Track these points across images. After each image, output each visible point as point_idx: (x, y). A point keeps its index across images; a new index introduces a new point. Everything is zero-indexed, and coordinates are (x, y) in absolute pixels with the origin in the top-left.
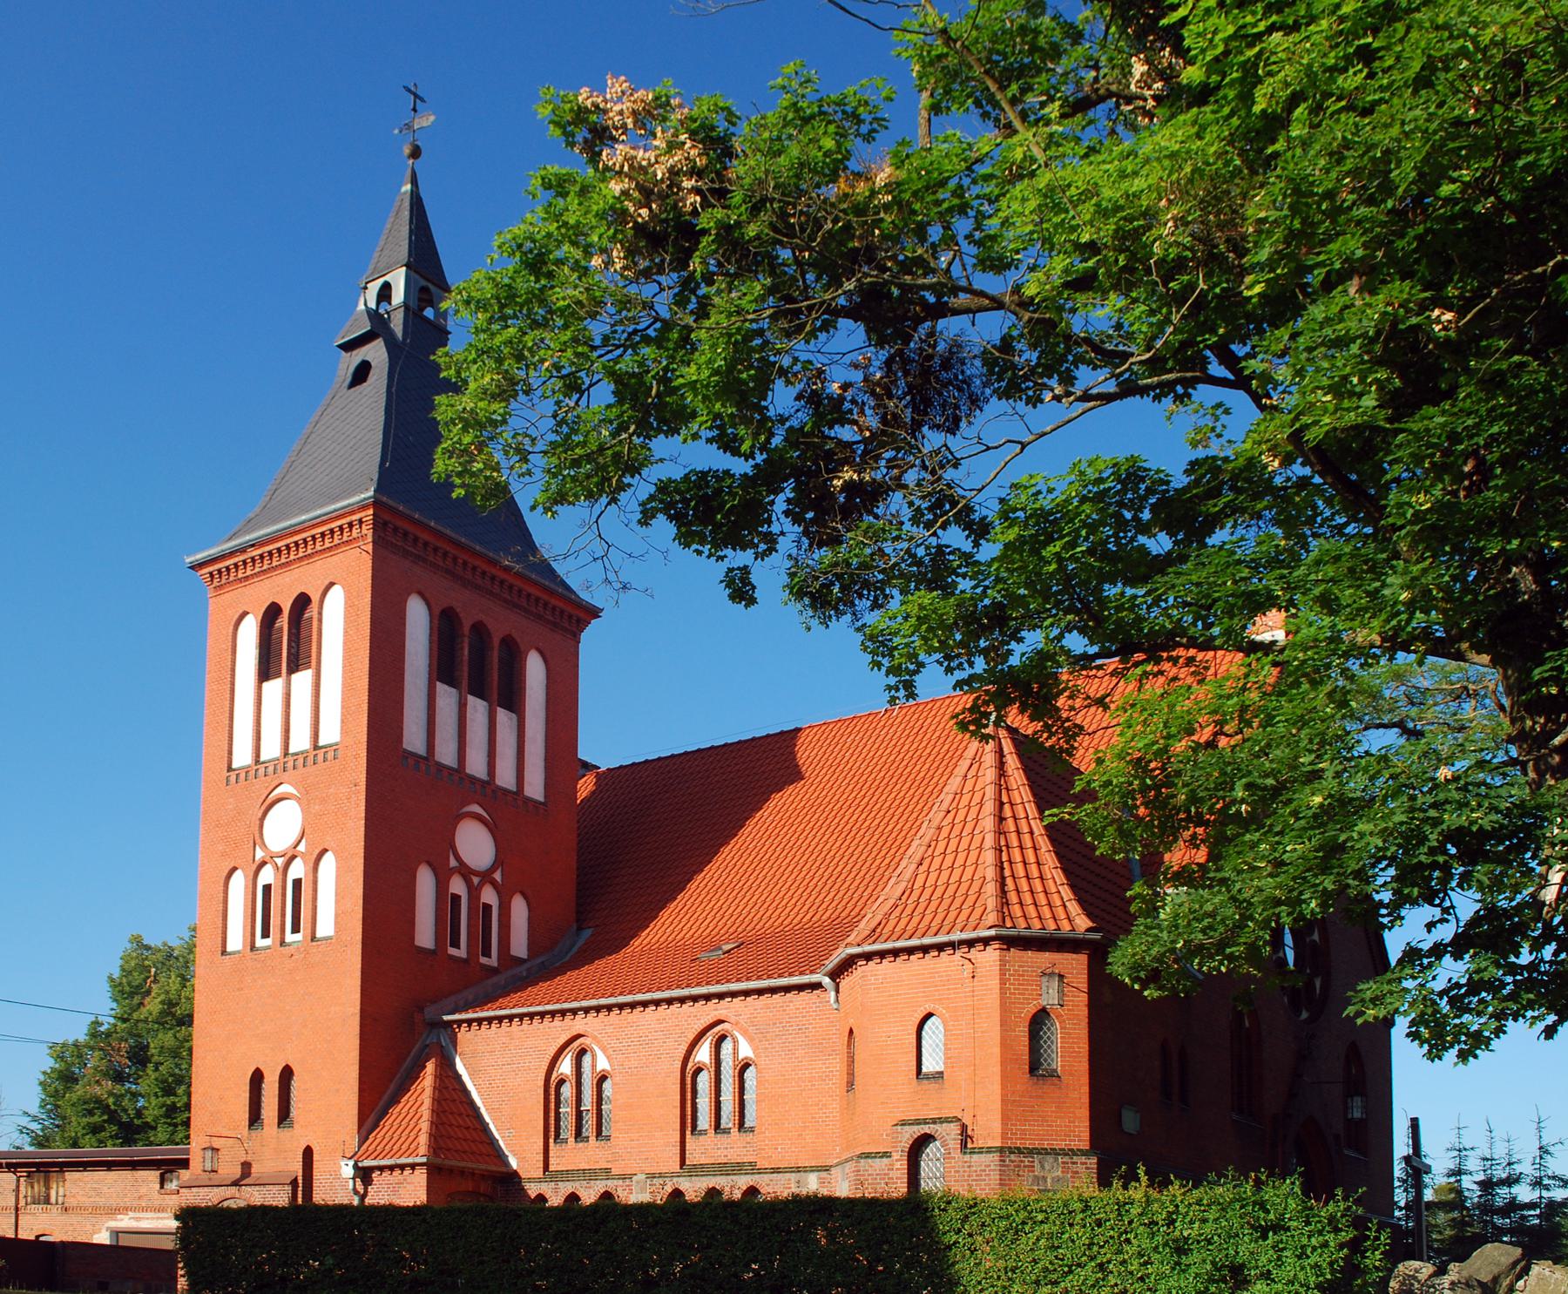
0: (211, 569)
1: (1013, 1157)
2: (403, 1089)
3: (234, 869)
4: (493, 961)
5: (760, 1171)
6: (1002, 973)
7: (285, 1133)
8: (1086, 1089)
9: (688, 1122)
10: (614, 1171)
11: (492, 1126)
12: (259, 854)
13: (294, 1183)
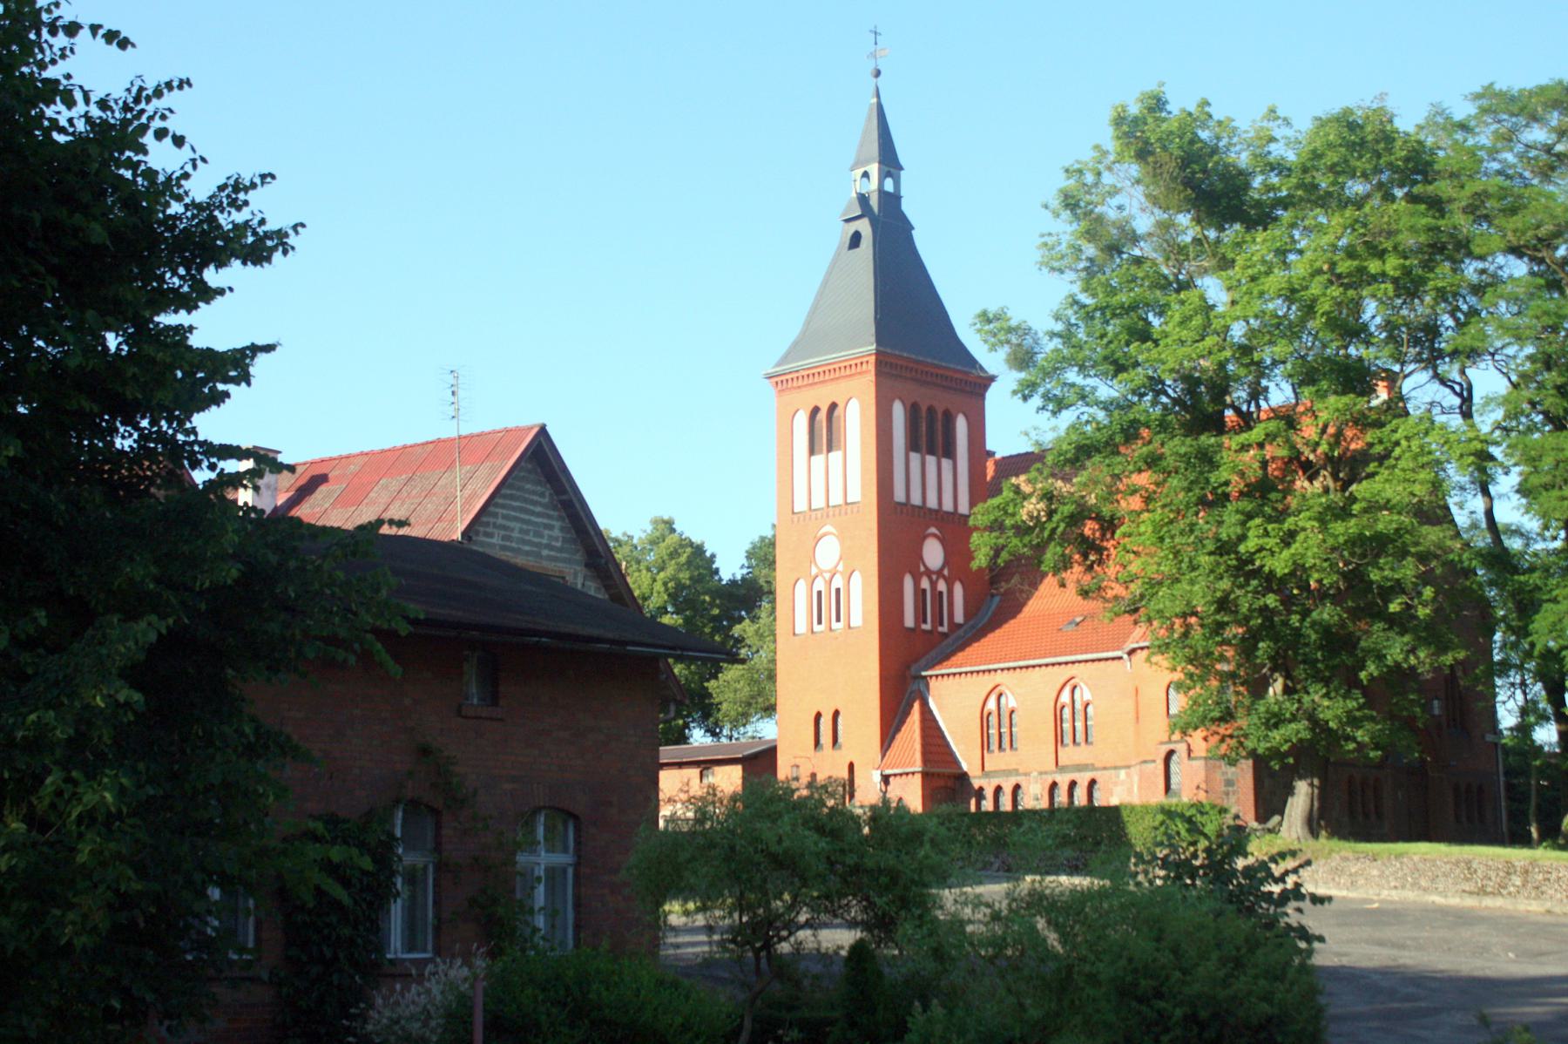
2: (902, 722)
7: (837, 753)
9: (1059, 739)
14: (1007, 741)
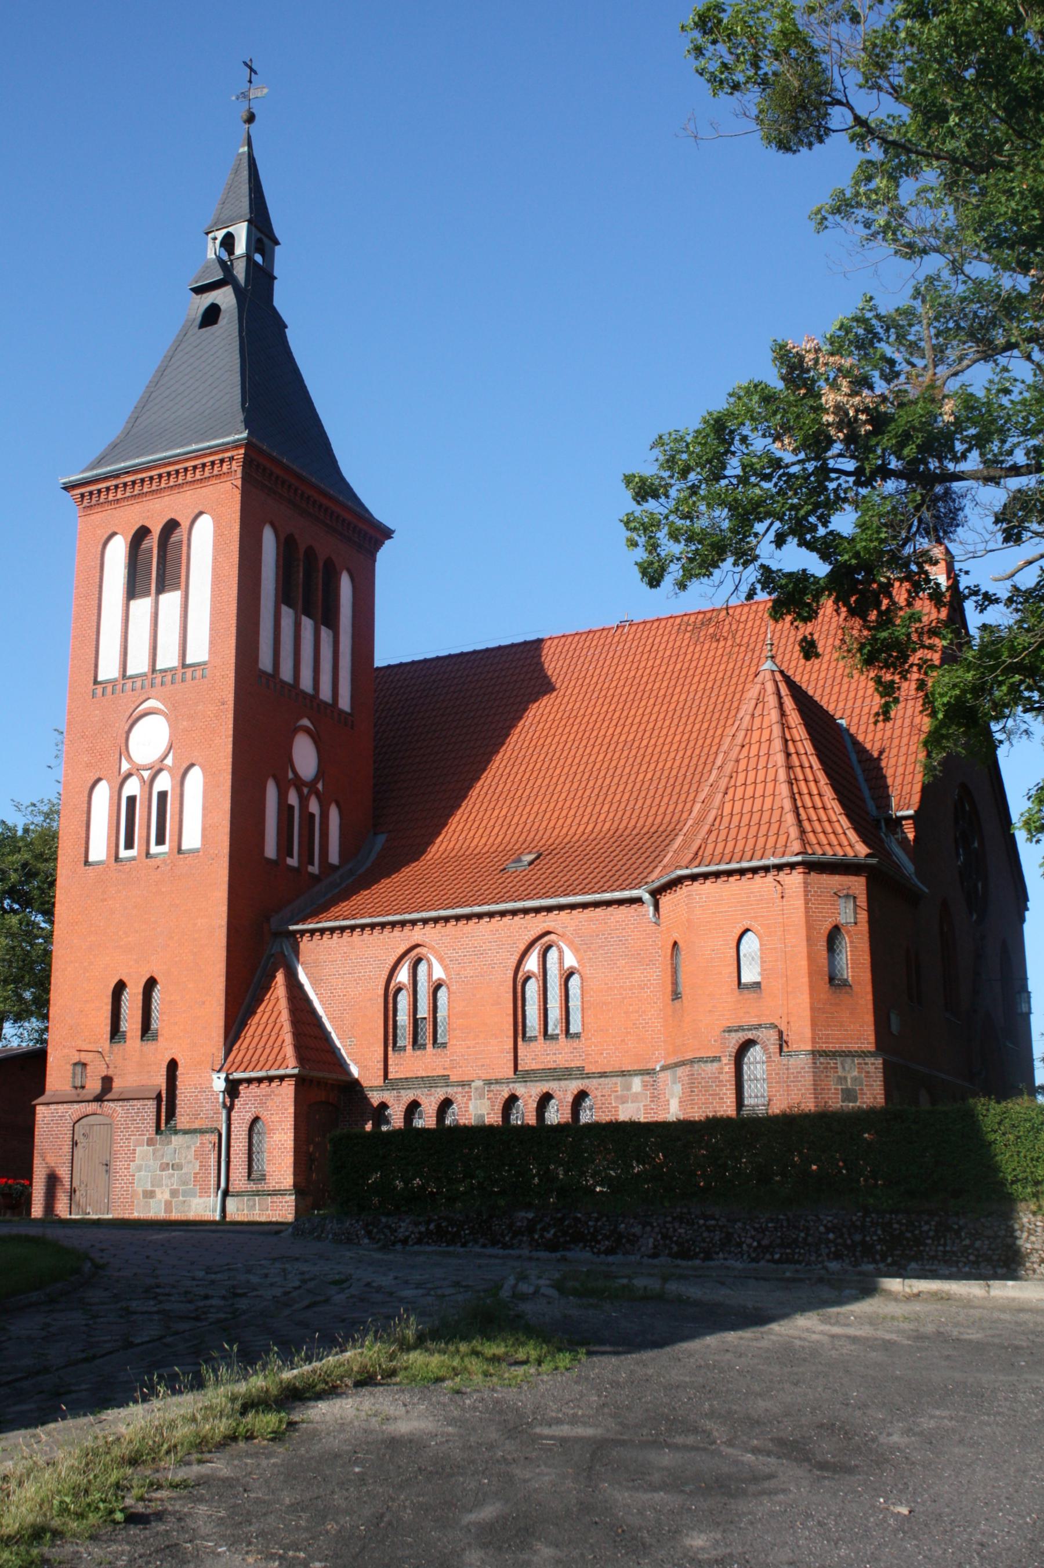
0: (82, 490)
1: (822, 1060)
2: (258, 1000)
3: (99, 780)
4: (314, 869)
5: (589, 1076)
6: (806, 892)
7: (149, 1047)
8: (870, 997)
10: (453, 1078)
11: (334, 1036)
12: (125, 766)
13: (159, 1097)
14: (425, 1033)
